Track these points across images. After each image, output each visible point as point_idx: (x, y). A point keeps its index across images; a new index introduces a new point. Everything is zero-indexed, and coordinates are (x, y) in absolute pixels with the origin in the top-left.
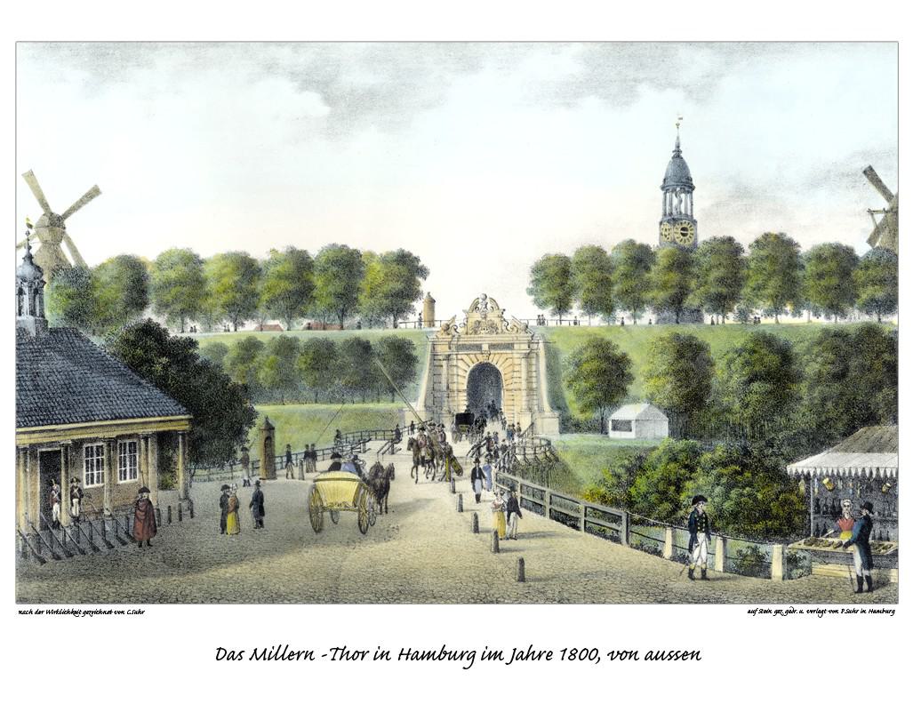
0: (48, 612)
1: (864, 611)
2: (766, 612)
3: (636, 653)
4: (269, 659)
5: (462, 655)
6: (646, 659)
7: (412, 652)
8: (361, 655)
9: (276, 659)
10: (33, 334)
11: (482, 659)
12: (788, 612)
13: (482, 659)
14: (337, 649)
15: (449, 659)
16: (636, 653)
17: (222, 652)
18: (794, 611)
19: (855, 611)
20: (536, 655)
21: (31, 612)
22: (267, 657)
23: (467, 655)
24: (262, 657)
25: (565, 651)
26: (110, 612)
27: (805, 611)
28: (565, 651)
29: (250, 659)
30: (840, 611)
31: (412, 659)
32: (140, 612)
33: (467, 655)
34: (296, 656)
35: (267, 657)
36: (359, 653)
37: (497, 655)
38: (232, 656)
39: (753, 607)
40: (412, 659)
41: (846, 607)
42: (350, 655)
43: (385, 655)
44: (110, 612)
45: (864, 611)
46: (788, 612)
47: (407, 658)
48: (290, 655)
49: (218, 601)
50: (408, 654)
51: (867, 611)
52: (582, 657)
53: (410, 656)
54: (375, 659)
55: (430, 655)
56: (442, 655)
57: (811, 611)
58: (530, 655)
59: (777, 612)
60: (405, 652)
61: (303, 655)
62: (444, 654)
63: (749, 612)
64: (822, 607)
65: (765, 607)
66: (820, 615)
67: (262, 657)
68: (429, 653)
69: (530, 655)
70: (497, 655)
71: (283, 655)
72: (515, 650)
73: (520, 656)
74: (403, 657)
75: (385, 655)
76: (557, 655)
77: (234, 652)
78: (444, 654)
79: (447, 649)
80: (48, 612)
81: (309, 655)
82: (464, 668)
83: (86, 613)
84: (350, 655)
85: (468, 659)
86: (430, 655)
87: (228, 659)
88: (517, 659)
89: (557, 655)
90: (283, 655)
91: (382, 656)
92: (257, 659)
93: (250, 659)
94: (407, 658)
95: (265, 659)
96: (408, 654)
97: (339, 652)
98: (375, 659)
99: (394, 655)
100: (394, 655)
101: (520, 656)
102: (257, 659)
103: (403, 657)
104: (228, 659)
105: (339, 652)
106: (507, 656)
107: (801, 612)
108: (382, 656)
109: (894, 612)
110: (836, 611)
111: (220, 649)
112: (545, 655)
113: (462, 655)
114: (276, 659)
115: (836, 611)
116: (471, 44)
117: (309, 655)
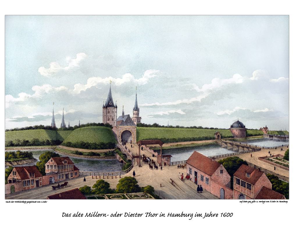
0: (15, 202)
1: (278, 202)
2: (245, 202)
3: (164, 214)
4: (91, 216)
5: (188, 215)
6: (73, 216)
7: (172, 214)
8: (155, 215)
9: (94, 216)
10: (185, 113)
11: (195, 216)
12: (253, 202)
13: (195, 216)
14: (148, 213)
15: (184, 216)
16: (164, 214)
17: (64, 214)
18: (255, 202)
19: (274, 202)
20: (212, 215)
21: (10, 202)
22: (91, 216)
23: (190, 215)
24: (87, 216)
25: (222, 214)
26: (36, 202)
27: (258, 202)
28: (222, 214)
29: (85, 216)
30: (270, 202)
31: (172, 216)
32: (45, 202)
33: (190, 215)
34: (140, 215)
35: (91, 216)
36: (155, 214)
37: (200, 215)
38: (67, 215)
39: (241, 200)
40: (172, 216)
41: (272, 200)
42: (152, 215)
43: (163, 215)
44: (36, 202)
45: (278, 202)
46: (253, 202)
47: (170, 216)
48: (98, 215)
49: (198, 199)
50: (171, 215)
51: (279, 202)
52: (228, 216)
53: (171, 216)
54: (160, 216)
55: (178, 215)
56: (182, 215)
57: (260, 202)
58: (211, 215)
59: (249, 202)
60: (170, 214)
61: (103, 215)
62: (183, 215)
63: (240, 202)
64: (264, 200)
65: (245, 200)
66: (263, 203)
67: (87, 216)
68: (177, 216)
69: (211, 215)
70: (200, 215)
71: (96, 215)
72: (206, 213)
73: (207, 215)
74: (169, 216)
75: (163, 215)
76: (220, 215)
77: (174, 214)
78: (183, 215)
79: (184, 213)
80: (15, 202)
81: (104, 215)
82: (203, 218)
83: (28, 202)
84: (152, 215)
85: (191, 216)
86: (178, 215)
87: (66, 216)
88: (206, 216)
89: (220, 215)
90: (96, 215)
91: (162, 215)
92: (88, 216)
93: (85, 216)
94: (170, 216)
95: (90, 216)
96: (171, 215)
97: (148, 214)
98: (160, 216)
99: (166, 215)
100: (166, 215)
101: (207, 215)
102: (88, 216)
103: (169, 216)
104: (66, 216)
105: (148, 214)
106: (203, 215)
107: (257, 202)
108: (162, 215)
109: (287, 202)
110: (40, 202)
111: (126, 213)
112: (216, 215)
113: (188, 215)
114: (94, 216)
115: (40, 202)
116: (6, 56)
117: (104, 215)
